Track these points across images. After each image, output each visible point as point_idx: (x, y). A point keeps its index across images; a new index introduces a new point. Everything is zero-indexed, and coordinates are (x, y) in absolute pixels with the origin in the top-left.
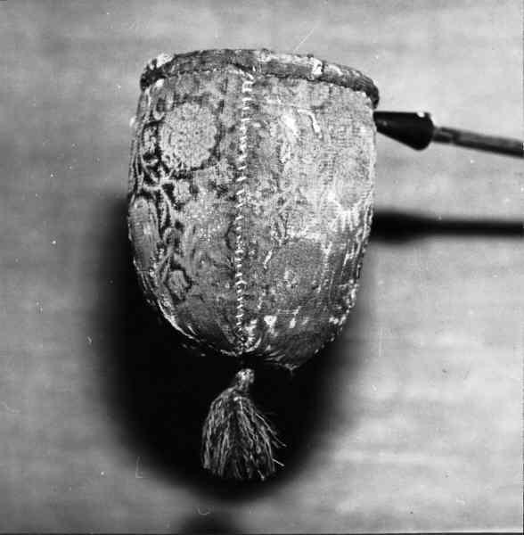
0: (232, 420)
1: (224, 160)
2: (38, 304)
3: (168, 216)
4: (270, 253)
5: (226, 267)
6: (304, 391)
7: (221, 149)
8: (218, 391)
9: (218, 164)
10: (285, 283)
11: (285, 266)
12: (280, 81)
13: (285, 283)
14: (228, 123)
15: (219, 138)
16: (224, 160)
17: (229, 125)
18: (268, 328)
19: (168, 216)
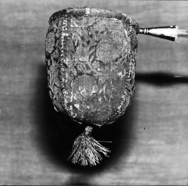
0: (90, 151)
1: (57, 49)
2: (112, 117)
3: (90, 58)
4: (72, 81)
5: (60, 87)
6: (117, 135)
7: (56, 46)
8: (77, 136)
9: (56, 51)
10: (80, 91)
11: (79, 85)
12: (76, 18)
13: (80, 91)
14: (58, 36)
15: (55, 42)
16: (57, 49)
17: (58, 37)
18: (78, 109)
19: (90, 58)
